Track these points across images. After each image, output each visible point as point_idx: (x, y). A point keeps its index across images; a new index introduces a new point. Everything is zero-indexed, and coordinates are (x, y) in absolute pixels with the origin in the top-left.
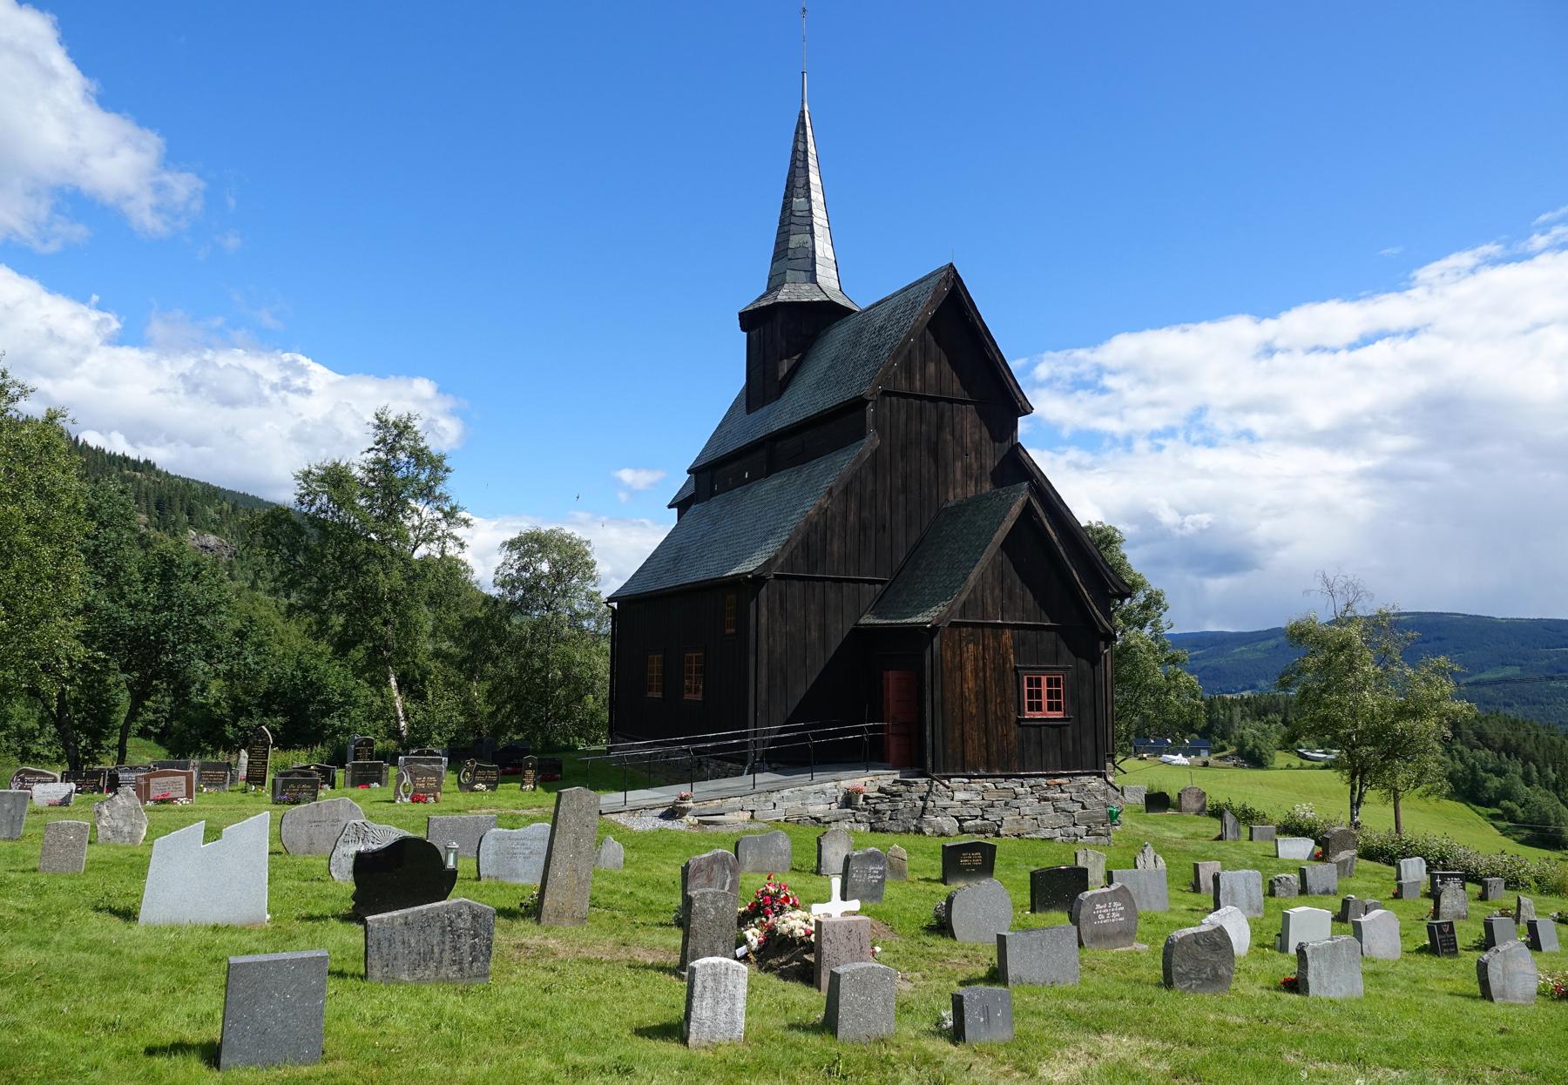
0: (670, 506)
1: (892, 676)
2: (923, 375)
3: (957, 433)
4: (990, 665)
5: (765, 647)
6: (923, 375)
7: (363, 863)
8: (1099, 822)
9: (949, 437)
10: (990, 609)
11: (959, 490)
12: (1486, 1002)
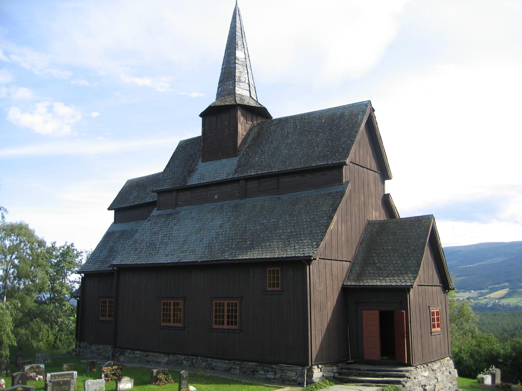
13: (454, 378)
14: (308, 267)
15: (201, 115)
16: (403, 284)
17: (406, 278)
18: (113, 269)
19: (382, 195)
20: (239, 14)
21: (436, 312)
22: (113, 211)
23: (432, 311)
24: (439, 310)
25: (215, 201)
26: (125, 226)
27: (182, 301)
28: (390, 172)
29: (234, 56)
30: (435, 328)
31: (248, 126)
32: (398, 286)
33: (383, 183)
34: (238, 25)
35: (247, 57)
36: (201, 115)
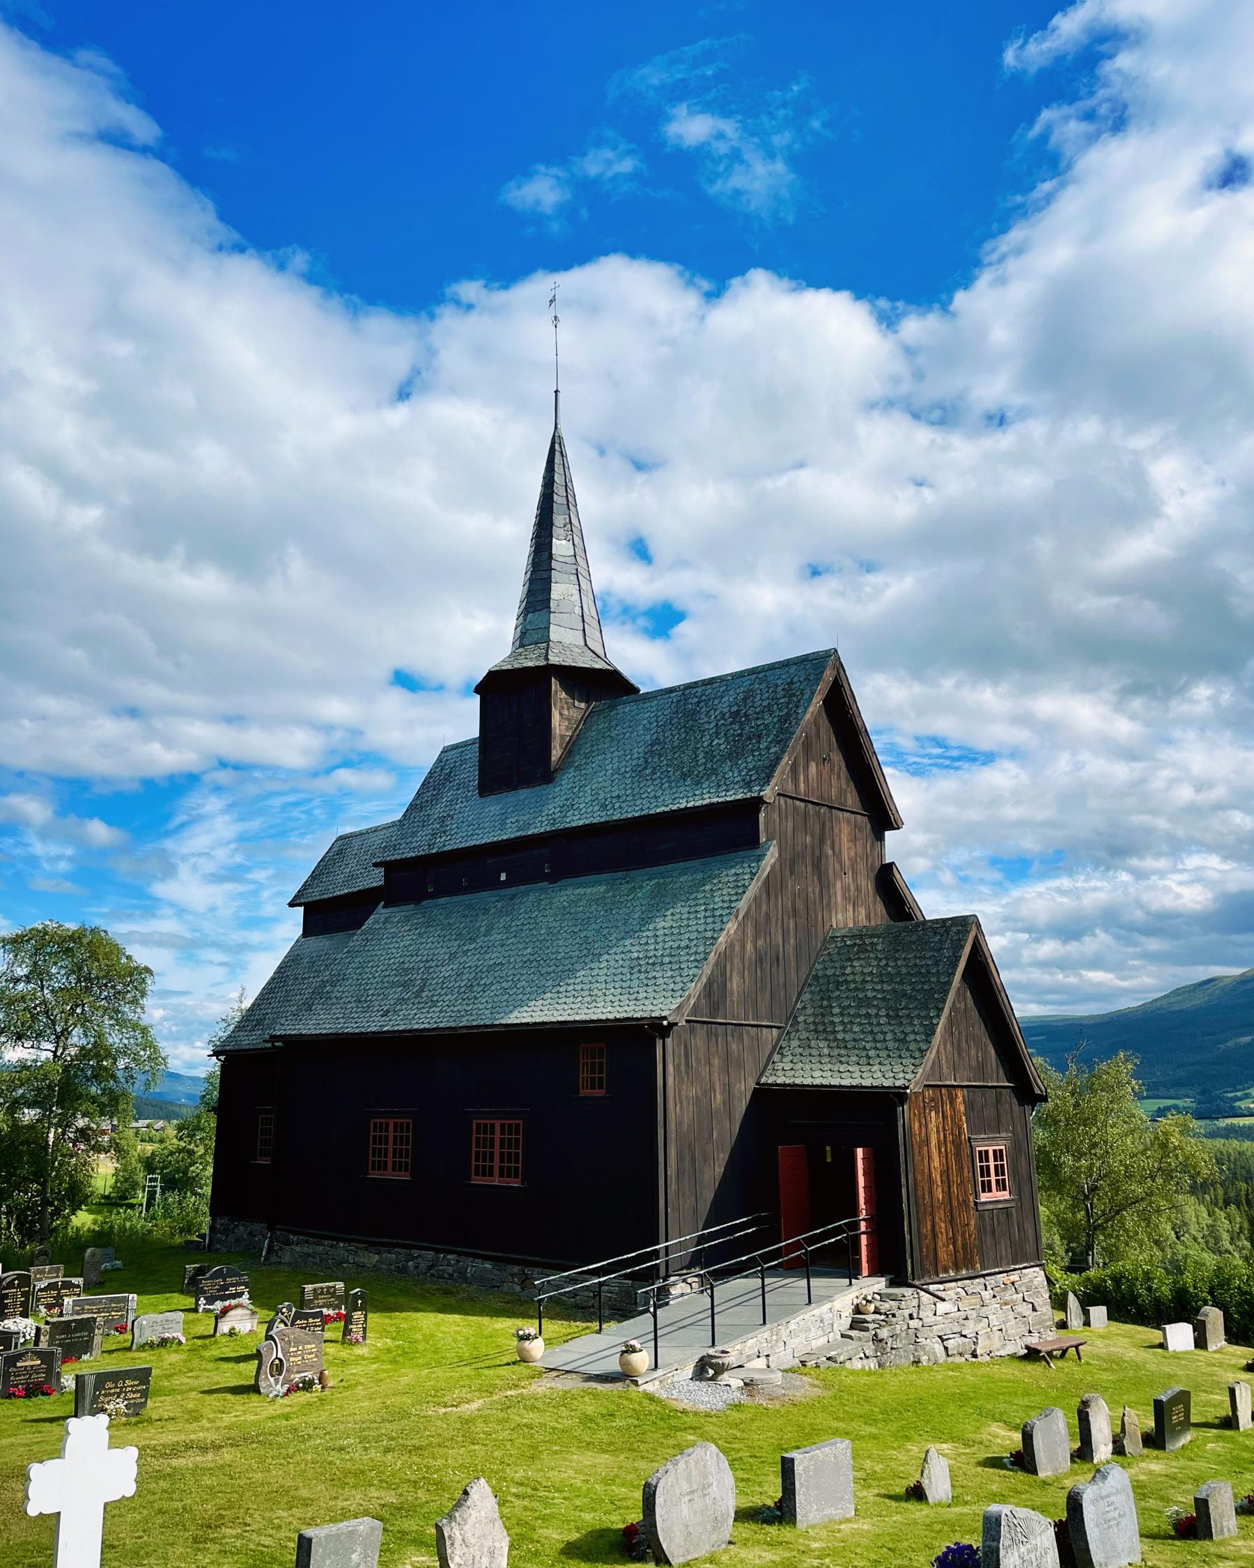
0: (291, 905)
1: (860, 1152)
2: (806, 777)
3: (837, 849)
4: (950, 1138)
5: (673, 1116)
6: (806, 777)
7: (310, 1540)
8: (1047, 1327)
9: (830, 852)
10: (945, 1070)
11: (840, 916)
12: (1021, 1476)
13: (1049, 1323)
14: (659, 1043)
15: (479, 689)
16: (844, 1083)
17: (898, 1068)
18: (274, 1047)
19: (878, 865)
20: (561, 452)
21: (995, 1151)
22: (300, 911)
23: (978, 1149)
24: (1003, 1147)
25: (501, 885)
26: (320, 943)
27: (521, 1122)
28: (894, 812)
29: (547, 553)
30: (990, 1191)
31: (576, 715)
32: (866, 1087)
33: (880, 838)
34: (558, 478)
35: (580, 552)
36: (479, 689)
